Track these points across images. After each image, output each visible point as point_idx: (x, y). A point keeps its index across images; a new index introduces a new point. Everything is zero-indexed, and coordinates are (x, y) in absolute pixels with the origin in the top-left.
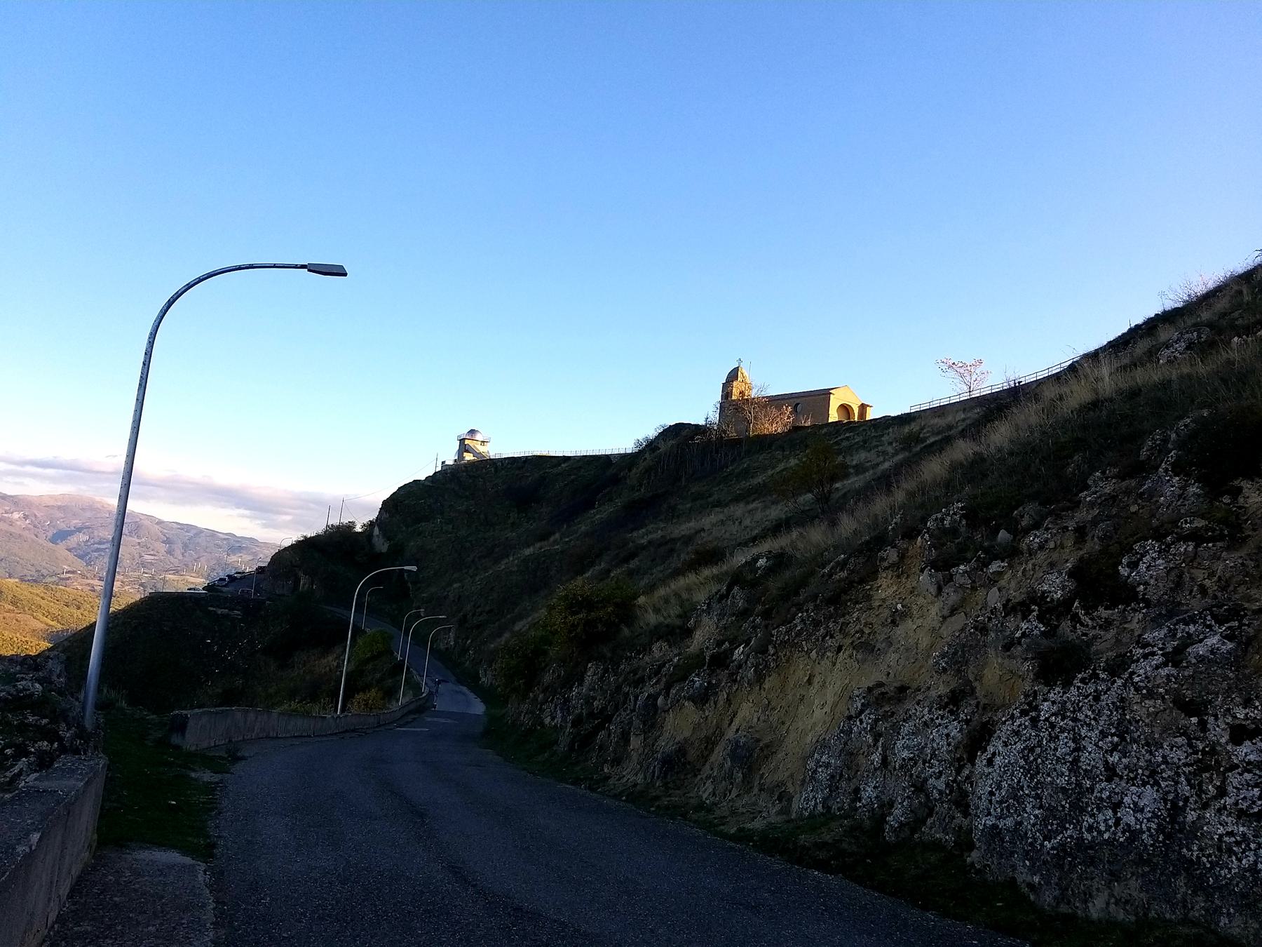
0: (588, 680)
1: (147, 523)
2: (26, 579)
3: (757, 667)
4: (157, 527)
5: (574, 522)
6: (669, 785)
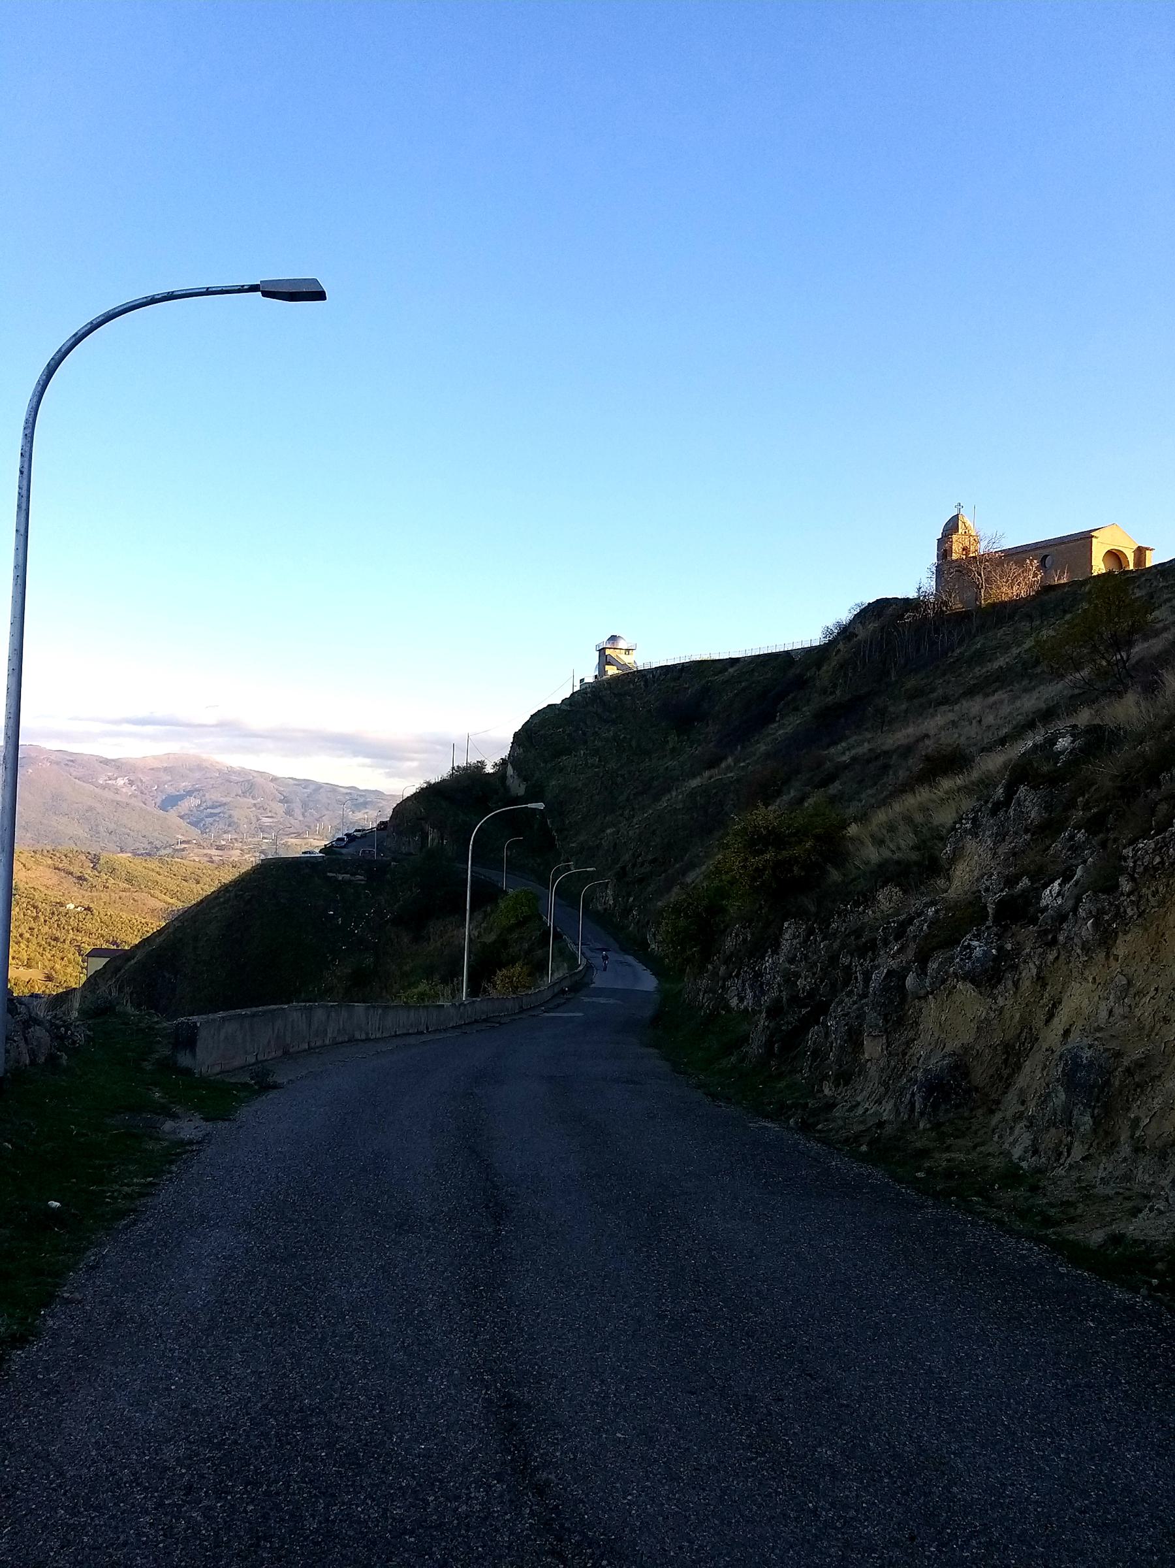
0: (785, 946)
1: (259, 780)
2: (139, 852)
3: (1098, 919)
4: (272, 784)
5: (749, 741)
6: (943, 1129)
